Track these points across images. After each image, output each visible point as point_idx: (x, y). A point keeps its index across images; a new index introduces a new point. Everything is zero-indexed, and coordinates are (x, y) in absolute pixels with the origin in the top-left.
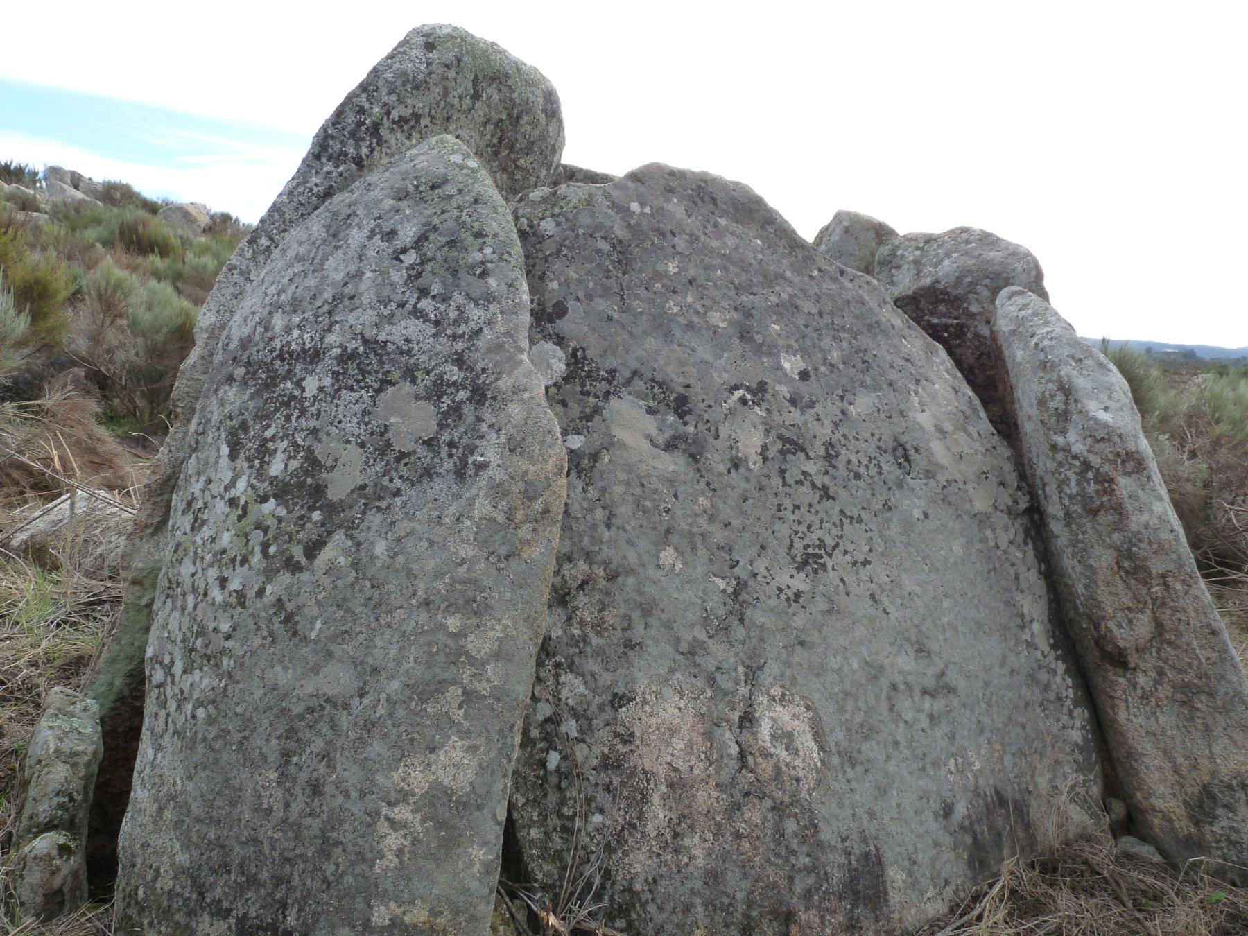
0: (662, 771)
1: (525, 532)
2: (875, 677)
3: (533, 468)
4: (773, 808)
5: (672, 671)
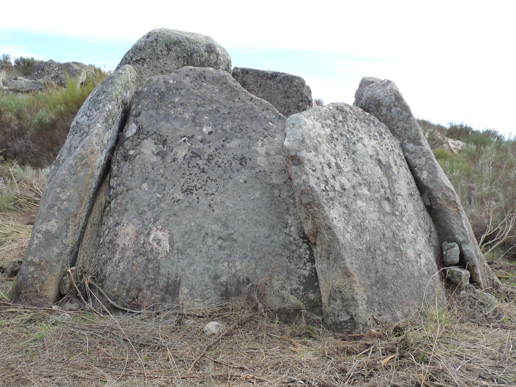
0: (121, 245)
1: (79, 168)
2: (200, 230)
3: (84, 152)
4: (147, 259)
5: (134, 218)
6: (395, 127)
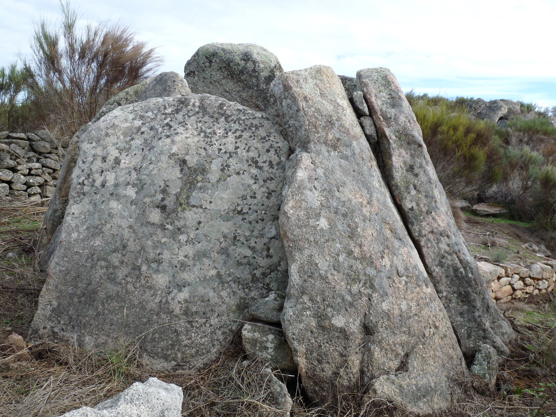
6: (287, 126)
